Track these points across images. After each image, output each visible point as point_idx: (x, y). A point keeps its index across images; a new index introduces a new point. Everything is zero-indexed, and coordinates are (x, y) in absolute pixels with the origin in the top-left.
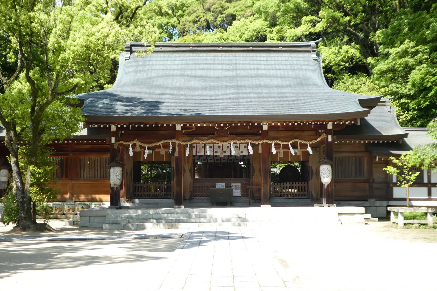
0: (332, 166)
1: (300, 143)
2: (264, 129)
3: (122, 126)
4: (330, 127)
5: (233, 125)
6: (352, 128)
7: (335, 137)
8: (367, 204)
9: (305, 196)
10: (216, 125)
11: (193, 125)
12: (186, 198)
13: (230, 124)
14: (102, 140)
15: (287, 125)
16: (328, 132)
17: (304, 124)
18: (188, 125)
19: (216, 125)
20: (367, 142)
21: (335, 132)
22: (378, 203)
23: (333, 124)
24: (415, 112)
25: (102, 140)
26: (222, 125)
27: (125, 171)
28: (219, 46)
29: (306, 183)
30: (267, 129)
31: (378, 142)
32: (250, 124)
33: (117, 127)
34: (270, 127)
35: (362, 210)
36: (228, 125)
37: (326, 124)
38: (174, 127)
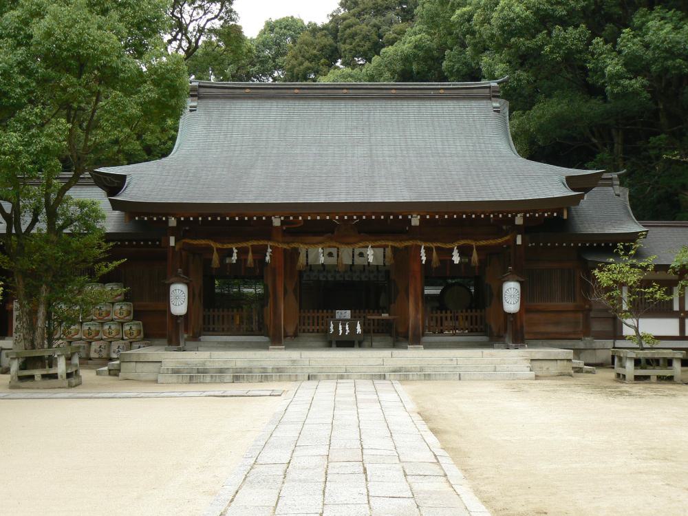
0: (522, 284)
1: (436, 247)
2: (413, 224)
5: (364, 217)
6: (548, 221)
8: (581, 345)
9: (477, 331)
10: (337, 218)
11: (300, 218)
12: (289, 334)
13: (359, 217)
14: (154, 241)
15: (451, 217)
16: (519, 230)
17: (478, 216)
18: (291, 218)
19: (337, 218)
20: (580, 245)
22: (599, 343)
23: (524, 217)
24: (6, 66)
25: (154, 241)
26: (346, 218)
28: (343, 89)
29: (483, 310)
30: (418, 224)
31: (591, 245)
32: (391, 217)
33: (179, 221)
34: (423, 220)
35: (568, 353)
36: (355, 217)
37: (514, 217)
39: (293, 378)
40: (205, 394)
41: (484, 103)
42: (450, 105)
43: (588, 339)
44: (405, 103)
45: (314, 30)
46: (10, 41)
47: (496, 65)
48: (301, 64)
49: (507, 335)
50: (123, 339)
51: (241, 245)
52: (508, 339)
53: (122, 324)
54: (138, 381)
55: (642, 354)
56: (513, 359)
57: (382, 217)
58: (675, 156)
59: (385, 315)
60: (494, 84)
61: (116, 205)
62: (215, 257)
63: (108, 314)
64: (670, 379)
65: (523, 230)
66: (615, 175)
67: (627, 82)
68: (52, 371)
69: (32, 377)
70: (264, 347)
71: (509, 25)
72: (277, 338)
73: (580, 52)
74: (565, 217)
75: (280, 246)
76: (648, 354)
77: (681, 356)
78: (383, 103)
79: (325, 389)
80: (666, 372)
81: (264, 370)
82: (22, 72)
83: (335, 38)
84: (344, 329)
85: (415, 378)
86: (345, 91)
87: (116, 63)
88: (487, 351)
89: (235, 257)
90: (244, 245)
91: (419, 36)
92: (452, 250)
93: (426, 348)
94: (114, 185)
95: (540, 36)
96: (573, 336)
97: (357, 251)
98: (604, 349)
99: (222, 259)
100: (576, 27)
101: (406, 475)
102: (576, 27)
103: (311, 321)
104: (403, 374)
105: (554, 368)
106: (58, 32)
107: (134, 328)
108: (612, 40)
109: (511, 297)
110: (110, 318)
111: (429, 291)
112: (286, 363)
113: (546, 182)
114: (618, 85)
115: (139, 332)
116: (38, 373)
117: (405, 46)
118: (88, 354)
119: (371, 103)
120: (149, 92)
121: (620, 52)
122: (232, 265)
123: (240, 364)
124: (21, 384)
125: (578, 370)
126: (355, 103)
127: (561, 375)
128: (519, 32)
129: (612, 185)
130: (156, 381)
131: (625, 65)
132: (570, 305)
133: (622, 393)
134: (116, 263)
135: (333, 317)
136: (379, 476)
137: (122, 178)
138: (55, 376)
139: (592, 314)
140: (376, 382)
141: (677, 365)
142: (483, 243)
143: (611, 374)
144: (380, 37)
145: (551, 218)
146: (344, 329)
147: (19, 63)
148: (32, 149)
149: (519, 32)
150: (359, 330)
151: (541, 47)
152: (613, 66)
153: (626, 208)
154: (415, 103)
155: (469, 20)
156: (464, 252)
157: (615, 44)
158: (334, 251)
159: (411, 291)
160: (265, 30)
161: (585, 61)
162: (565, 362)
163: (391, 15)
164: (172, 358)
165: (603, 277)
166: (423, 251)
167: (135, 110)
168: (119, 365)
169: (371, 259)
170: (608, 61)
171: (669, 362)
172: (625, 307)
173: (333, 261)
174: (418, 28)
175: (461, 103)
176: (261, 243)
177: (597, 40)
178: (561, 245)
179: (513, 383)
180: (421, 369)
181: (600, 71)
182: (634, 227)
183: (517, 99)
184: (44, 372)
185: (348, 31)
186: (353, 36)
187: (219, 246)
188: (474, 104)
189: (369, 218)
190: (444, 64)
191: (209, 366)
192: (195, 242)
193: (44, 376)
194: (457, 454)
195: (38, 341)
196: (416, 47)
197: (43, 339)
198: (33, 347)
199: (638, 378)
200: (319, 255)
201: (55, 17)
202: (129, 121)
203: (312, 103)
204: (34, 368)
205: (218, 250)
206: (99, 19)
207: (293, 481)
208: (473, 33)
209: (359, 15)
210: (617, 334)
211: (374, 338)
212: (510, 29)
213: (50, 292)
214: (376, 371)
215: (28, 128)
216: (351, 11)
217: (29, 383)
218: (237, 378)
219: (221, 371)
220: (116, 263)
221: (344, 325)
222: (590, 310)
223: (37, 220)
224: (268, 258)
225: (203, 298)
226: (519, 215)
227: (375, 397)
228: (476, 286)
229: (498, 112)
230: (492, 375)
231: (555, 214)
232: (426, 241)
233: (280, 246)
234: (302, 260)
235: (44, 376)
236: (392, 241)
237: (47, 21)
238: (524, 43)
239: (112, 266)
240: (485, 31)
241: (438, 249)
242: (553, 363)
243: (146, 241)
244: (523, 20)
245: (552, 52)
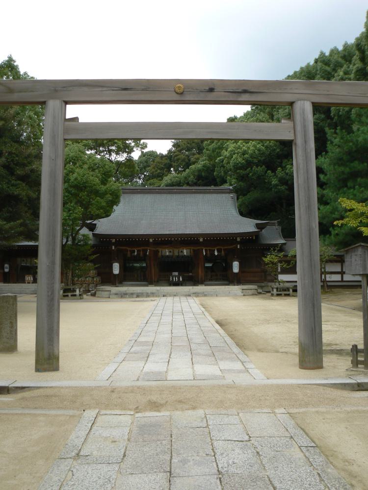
0: (240, 262)
8: (263, 284)
34: (204, 240)
41: (227, 195)
42: (215, 196)
43: (266, 282)
44: (198, 195)
45: (162, 156)
47: (232, 182)
48: (156, 171)
53: (93, 278)
54: (102, 297)
56: (236, 289)
59: (190, 274)
60: (231, 188)
62: (129, 253)
64: (288, 295)
65: (240, 243)
66: (276, 222)
67: (280, 187)
68: (75, 293)
69: (67, 296)
70: (147, 286)
71: (237, 166)
72: (150, 282)
73: (263, 176)
79: (170, 299)
80: (287, 293)
81: (147, 293)
84: (176, 280)
87: (98, 188)
88: (227, 287)
89: (136, 253)
90: (139, 249)
91: (205, 162)
92: (215, 250)
93: (205, 285)
94: (92, 227)
95: (248, 170)
97: (180, 251)
99: (131, 254)
100: (261, 167)
102: (261, 167)
104: (197, 295)
105: (250, 292)
106: (79, 179)
107: (98, 279)
108: (274, 171)
109: (236, 267)
111: (207, 265)
113: (248, 226)
114: (276, 188)
115: (100, 281)
116: (70, 294)
117: (199, 165)
119: (185, 195)
120: (109, 197)
122: (134, 256)
123: (138, 292)
124: (64, 298)
125: (260, 293)
127: (253, 295)
128: (240, 168)
129: (275, 225)
130: (109, 298)
131: (279, 181)
133: (272, 299)
134: (95, 256)
135: (172, 274)
137: (95, 224)
138: (75, 295)
140: (187, 297)
142: (226, 247)
143: (270, 294)
144: (189, 160)
145: (249, 239)
146: (176, 280)
148: (71, 218)
149: (240, 168)
150: (181, 280)
152: (274, 181)
153: (280, 234)
154: (201, 195)
155: (223, 162)
157: (275, 173)
158: (171, 250)
160: (141, 156)
161: (265, 179)
164: (114, 289)
166: (204, 250)
167: (104, 204)
168: (95, 292)
169: (185, 254)
170: (273, 179)
172: (279, 270)
173: (171, 254)
174: (204, 158)
175: (219, 195)
176: (146, 248)
177: (269, 171)
179: (235, 296)
180: (203, 293)
181: (270, 183)
182: (282, 241)
183: (239, 192)
184: (72, 294)
185: (176, 158)
186: (178, 160)
187: (130, 249)
189: (184, 239)
190: (215, 173)
191: (128, 292)
193: (72, 295)
194: (208, 311)
195: (69, 283)
196: (203, 166)
198: (68, 285)
199: (278, 295)
200: (167, 252)
201: (78, 173)
202: (102, 208)
203: (163, 195)
204: (68, 292)
205: (130, 251)
206: (91, 173)
208: (224, 167)
209: (180, 151)
212: (237, 167)
214: (187, 293)
215: (70, 210)
216: (177, 149)
217: (66, 298)
219: (132, 294)
221: (175, 278)
224: (148, 253)
225: (123, 268)
228: (225, 264)
230: (228, 295)
234: (160, 254)
235: (72, 295)
237: (75, 175)
238: (242, 172)
240: (228, 167)
241: (209, 249)
244: (242, 164)
245: (252, 176)
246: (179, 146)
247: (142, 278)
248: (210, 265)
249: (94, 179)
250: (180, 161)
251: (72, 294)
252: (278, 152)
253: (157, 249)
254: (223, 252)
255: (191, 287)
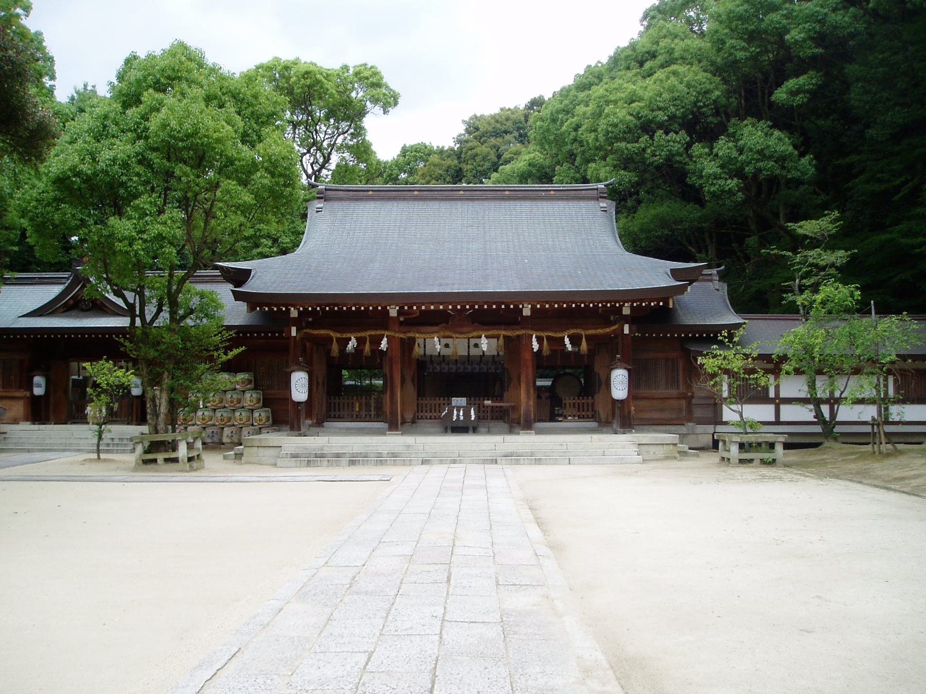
0: (629, 371)
3: (306, 310)
4: (626, 311)
5: (476, 307)
6: (653, 312)
7: (634, 328)
8: (683, 430)
9: (588, 417)
11: (415, 308)
13: (472, 307)
16: (626, 319)
18: (406, 308)
19: (450, 307)
21: (636, 319)
22: (700, 428)
23: (632, 306)
26: (459, 307)
27: (315, 378)
31: (694, 336)
32: (503, 307)
34: (533, 309)
36: (468, 307)
37: (621, 306)
38: (385, 312)
39: (408, 463)
40: (317, 478)
41: (591, 204)
42: (561, 205)
44: (518, 203)
45: (441, 152)
46: (129, 134)
49: (615, 421)
50: (252, 425)
51: (359, 335)
52: (615, 426)
55: (745, 439)
56: (621, 444)
57: (494, 307)
58: (773, 249)
60: (601, 186)
61: (238, 296)
62: (335, 347)
63: (239, 401)
64: (772, 463)
66: (714, 271)
68: (173, 455)
69: (154, 461)
70: (381, 433)
74: (671, 306)
75: (397, 335)
76: (752, 438)
77: (783, 440)
78: (497, 204)
79: (437, 471)
81: (380, 455)
82: (140, 162)
83: (459, 158)
84: (458, 415)
85: (526, 462)
86: (462, 193)
87: (232, 152)
88: (596, 437)
91: (532, 155)
94: (239, 278)
96: (676, 422)
98: (704, 434)
100: (677, 133)
101: (498, 584)
103: (428, 409)
105: (660, 451)
106: (174, 123)
109: (619, 384)
110: (241, 405)
111: (540, 383)
112: (401, 448)
113: (653, 274)
115: (268, 420)
116: (160, 457)
117: (520, 164)
118: (221, 439)
119: (486, 203)
121: (717, 155)
124: (145, 467)
125: (683, 453)
126: (471, 203)
127: (667, 458)
129: (711, 281)
130: (275, 465)
132: (674, 392)
134: (236, 351)
135: (449, 404)
136: (464, 587)
137: (248, 272)
138: (176, 460)
139: (694, 401)
140: (487, 466)
141: (779, 449)
146: (458, 415)
147: (137, 154)
151: (644, 150)
152: (710, 167)
154: (528, 204)
156: (575, 340)
159: (523, 377)
162: (671, 447)
163: (508, 137)
164: (290, 442)
165: (709, 363)
166: (534, 339)
171: (772, 446)
176: (378, 332)
178: (665, 335)
180: (532, 454)
183: (623, 199)
184: (167, 456)
187: (339, 335)
188: (583, 204)
192: (316, 332)
195: (161, 426)
196: (530, 165)
197: (166, 424)
199: (741, 461)
203: (431, 203)
205: (338, 339)
207: (357, 593)
210: (717, 420)
211: (491, 425)
213: (173, 379)
218: (352, 463)
219: (338, 456)
220: (236, 351)
221: (458, 411)
222: (692, 397)
223: (162, 310)
226: (626, 304)
227: (483, 482)
229: (605, 211)
231: (661, 304)
232: (536, 330)
233: (397, 335)
234: (418, 351)
236: (505, 330)
239: (231, 354)
241: (548, 338)
242: (660, 447)
243: (273, 333)
246: (477, 129)
247: (373, 413)
248: (547, 383)
249: (221, 126)
250: (478, 159)
251: (167, 456)
252: (718, 97)
253: (411, 335)
254: (584, 346)
255: (498, 439)
